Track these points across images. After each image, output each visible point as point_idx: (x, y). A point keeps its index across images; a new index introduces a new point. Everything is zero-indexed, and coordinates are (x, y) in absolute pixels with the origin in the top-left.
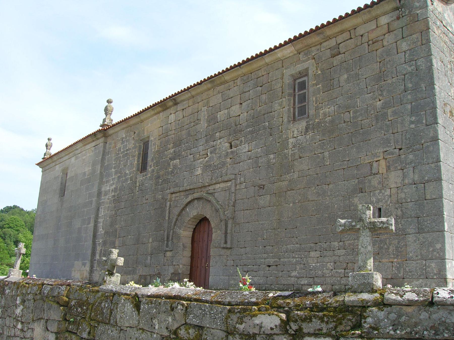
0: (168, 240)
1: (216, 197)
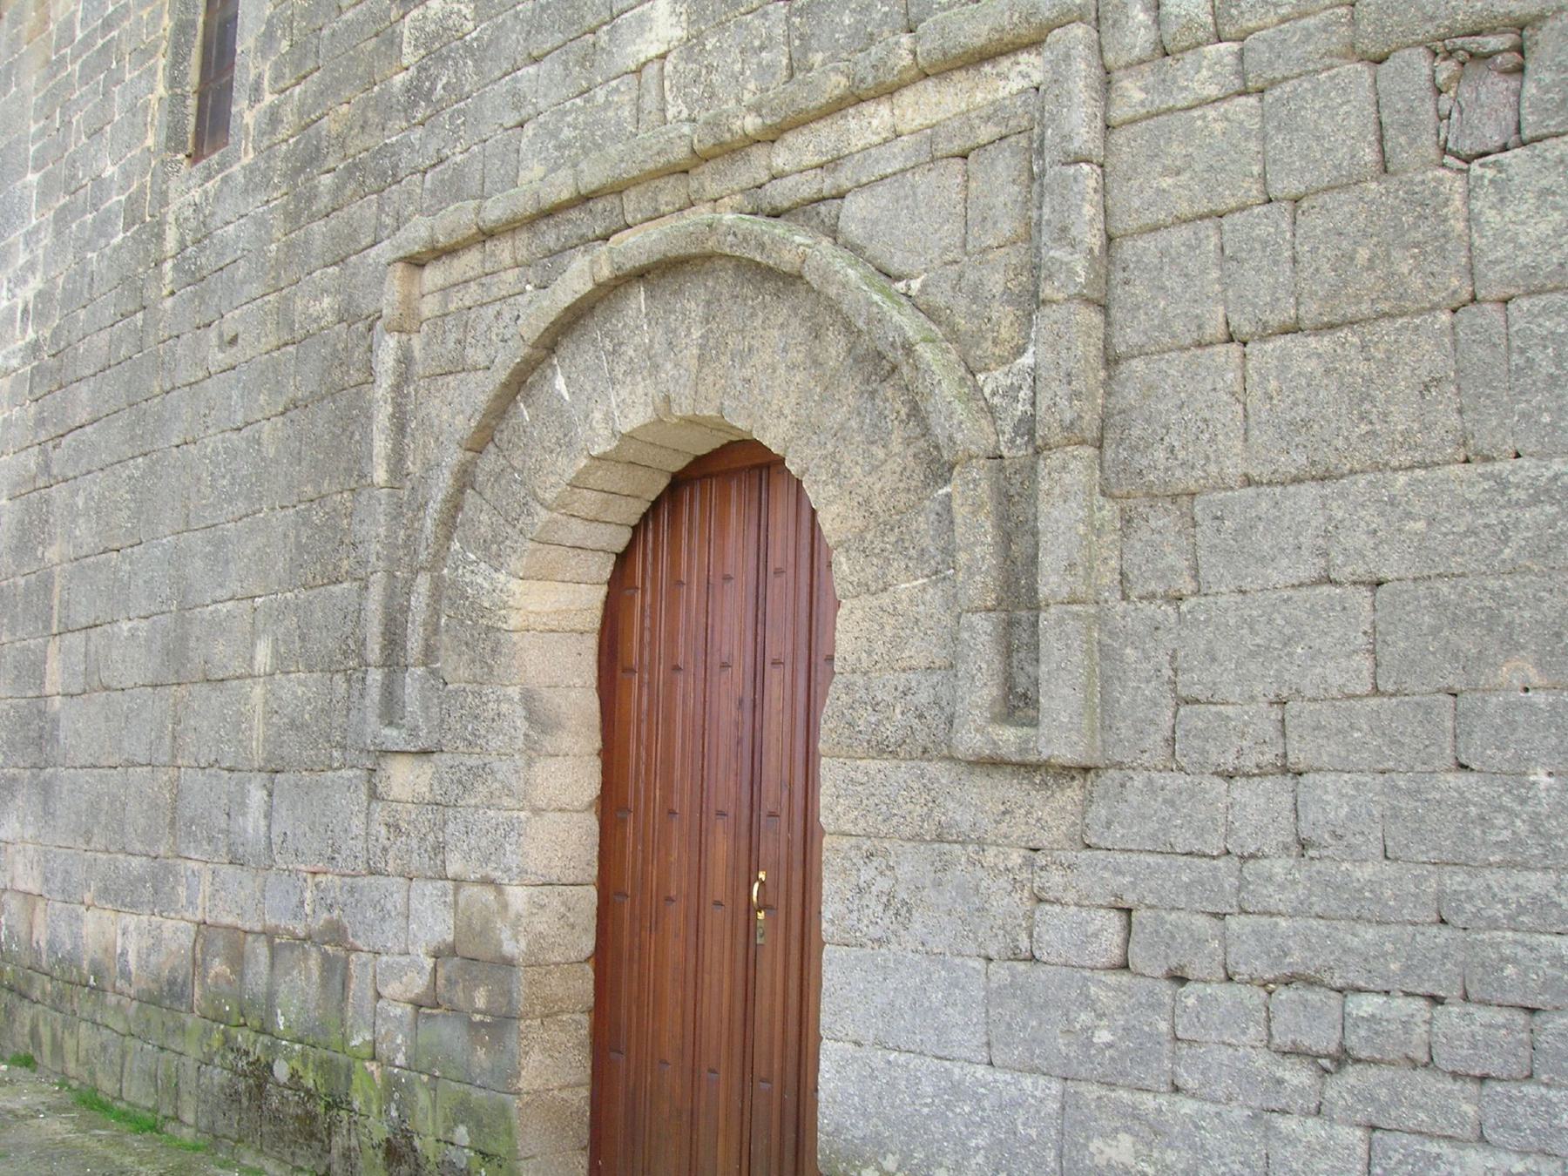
0: (393, 659)
1: (853, 229)
